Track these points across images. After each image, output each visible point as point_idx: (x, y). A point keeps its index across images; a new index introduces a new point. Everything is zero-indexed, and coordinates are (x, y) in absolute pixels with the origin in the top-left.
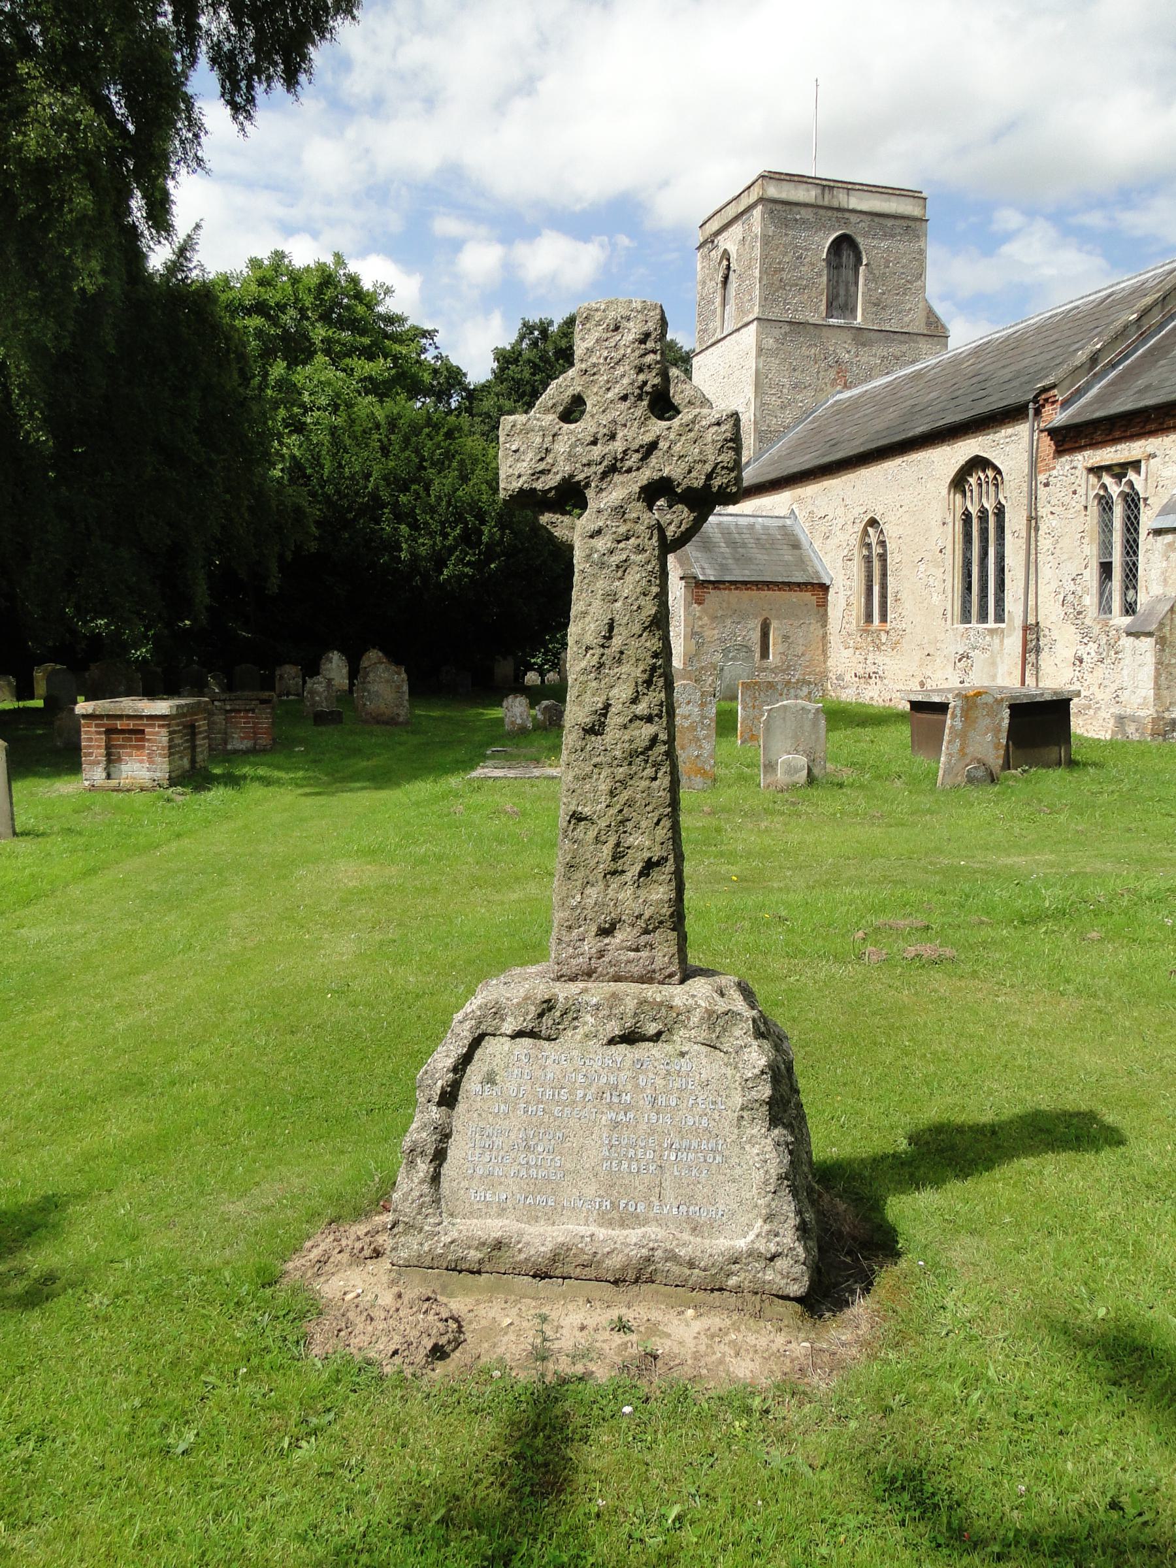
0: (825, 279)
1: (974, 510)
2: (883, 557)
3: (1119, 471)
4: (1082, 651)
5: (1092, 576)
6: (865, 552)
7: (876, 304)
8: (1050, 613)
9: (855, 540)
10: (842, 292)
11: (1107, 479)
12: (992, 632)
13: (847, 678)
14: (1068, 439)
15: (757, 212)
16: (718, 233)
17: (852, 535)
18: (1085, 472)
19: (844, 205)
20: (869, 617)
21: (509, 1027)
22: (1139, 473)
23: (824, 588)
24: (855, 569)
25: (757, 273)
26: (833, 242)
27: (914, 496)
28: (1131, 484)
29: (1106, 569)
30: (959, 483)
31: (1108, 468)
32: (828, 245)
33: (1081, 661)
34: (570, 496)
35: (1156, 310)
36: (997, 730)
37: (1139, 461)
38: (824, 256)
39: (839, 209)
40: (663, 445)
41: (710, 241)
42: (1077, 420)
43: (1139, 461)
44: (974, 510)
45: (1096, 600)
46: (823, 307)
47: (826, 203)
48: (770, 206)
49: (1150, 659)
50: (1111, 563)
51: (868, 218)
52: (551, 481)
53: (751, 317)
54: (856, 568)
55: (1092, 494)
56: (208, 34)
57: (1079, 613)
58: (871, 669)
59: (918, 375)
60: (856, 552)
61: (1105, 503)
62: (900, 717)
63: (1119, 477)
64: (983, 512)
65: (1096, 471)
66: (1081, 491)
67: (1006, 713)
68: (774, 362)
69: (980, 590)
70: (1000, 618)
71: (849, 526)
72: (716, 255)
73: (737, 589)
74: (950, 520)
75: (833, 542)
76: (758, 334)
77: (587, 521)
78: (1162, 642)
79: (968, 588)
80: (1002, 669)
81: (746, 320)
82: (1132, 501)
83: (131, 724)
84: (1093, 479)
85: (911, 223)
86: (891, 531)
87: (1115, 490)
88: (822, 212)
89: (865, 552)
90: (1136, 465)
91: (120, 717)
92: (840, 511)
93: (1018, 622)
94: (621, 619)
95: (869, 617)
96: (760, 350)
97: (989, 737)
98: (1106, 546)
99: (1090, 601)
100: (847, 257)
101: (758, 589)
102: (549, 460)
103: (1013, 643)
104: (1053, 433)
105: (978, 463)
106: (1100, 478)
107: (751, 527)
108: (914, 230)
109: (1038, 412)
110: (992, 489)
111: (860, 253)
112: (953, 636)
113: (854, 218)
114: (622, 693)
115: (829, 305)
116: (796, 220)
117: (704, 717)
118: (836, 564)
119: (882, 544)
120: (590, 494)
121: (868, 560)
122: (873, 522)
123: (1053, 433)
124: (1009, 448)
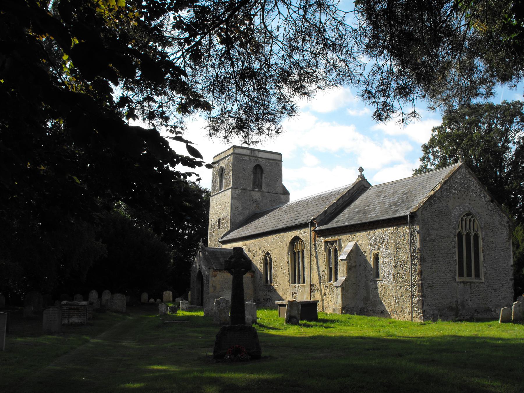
0: (252, 177)
10: (257, 181)
12: (302, 286)
13: (261, 300)
14: (320, 233)
19: (257, 156)
25: (231, 174)
29: (330, 269)
31: (330, 242)
35: (341, 200)
36: (298, 310)
39: (256, 157)
46: (252, 185)
47: (252, 155)
48: (235, 155)
51: (264, 160)
53: (229, 187)
64: (299, 252)
67: (300, 306)
68: (236, 201)
69: (296, 277)
75: (256, 258)
76: (231, 192)
80: (305, 297)
83: (75, 307)
88: (251, 158)
91: (73, 305)
93: (309, 283)
96: (232, 198)
97: (296, 312)
100: (259, 171)
103: (308, 289)
104: (316, 231)
113: (260, 160)
115: (254, 185)
117: (226, 306)
118: (257, 262)
122: (268, 253)
123: (316, 231)
124: (304, 234)
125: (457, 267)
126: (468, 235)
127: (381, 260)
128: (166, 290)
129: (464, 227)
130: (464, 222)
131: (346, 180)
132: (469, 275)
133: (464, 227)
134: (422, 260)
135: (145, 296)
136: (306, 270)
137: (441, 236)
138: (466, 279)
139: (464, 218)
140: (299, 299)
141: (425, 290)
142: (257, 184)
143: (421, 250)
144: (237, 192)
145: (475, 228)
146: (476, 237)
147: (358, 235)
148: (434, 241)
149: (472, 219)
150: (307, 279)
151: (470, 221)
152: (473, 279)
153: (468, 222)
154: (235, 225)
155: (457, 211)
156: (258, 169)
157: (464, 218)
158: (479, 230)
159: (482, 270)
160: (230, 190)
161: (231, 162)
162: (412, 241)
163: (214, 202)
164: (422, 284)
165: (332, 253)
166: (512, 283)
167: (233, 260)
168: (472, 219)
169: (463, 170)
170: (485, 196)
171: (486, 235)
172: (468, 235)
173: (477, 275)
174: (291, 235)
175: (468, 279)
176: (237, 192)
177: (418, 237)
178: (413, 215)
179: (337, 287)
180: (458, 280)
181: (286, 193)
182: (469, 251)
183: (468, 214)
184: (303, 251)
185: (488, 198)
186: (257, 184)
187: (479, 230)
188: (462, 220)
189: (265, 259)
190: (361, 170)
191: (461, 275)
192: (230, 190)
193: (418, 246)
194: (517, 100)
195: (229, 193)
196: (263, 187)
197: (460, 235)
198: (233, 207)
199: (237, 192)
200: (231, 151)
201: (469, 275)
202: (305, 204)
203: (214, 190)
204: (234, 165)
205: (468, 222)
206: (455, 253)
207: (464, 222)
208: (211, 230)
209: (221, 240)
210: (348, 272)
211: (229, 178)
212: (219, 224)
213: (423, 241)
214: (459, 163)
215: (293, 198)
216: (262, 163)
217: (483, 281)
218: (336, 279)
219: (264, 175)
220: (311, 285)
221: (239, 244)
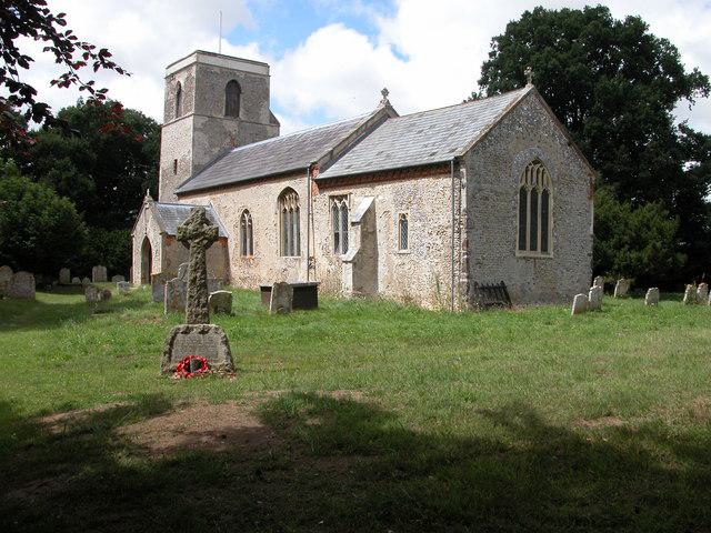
1: (529, 189)
2: (251, 227)
3: (340, 198)
5: (331, 239)
8: (319, 253)
14: (323, 185)
15: (194, 68)
16: (176, 73)
23: (226, 239)
27: (263, 202)
29: (337, 235)
30: (282, 197)
41: (170, 77)
44: (529, 189)
49: (351, 271)
59: (265, 146)
61: (335, 208)
62: (255, 293)
64: (291, 209)
65: (332, 197)
68: (200, 134)
69: (290, 244)
70: (299, 254)
72: (174, 83)
75: (229, 219)
78: (355, 264)
79: (245, 240)
80: (301, 275)
82: (344, 208)
86: (254, 215)
87: (339, 205)
95: (245, 253)
98: (337, 227)
99: (332, 248)
103: (304, 264)
104: (316, 181)
105: (289, 190)
109: (311, 172)
112: (279, 263)
118: (229, 229)
119: (250, 221)
121: (244, 227)
122: (246, 211)
123: (316, 181)
124: (301, 185)
125: (518, 235)
126: (534, 192)
127: (410, 225)
128: (96, 265)
129: (540, 181)
130: (529, 173)
131: (361, 108)
132: (533, 248)
133: (540, 181)
134: (469, 228)
135: (65, 273)
136: (306, 244)
137: (496, 193)
138: (527, 253)
139: (530, 167)
140: (290, 281)
141: (471, 269)
142: (232, 111)
143: (468, 211)
144: (203, 120)
145: (545, 182)
146: (546, 195)
147: (379, 188)
148: (487, 199)
149: (541, 169)
150: (304, 249)
151: (538, 172)
152: (538, 253)
153: (535, 173)
154: (198, 170)
155: (522, 157)
156: (234, 87)
157: (530, 167)
158: (550, 185)
159: (551, 241)
160: (191, 118)
161: (194, 74)
162: (455, 200)
163: (167, 137)
164: (467, 260)
165: (340, 212)
166: (590, 259)
167: (190, 227)
168: (541, 169)
169: (533, 98)
170: (560, 137)
171: (560, 192)
172: (534, 192)
173: (544, 249)
174: (278, 187)
175: (532, 254)
176: (202, 121)
177: (464, 192)
178: (458, 161)
179: (346, 262)
180: (517, 254)
181: (275, 123)
182: (533, 212)
183: (535, 162)
184: (298, 209)
185: (565, 140)
186: (232, 111)
187: (550, 185)
188: (527, 171)
189: (243, 220)
190: (385, 92)
191: (522, 247)
192: (191, 118)
193: (464, 206)
194: (480, 70)
195: (189, 122)
196: (241, 113)
197: (523, 192)
198: (197, 143)
199: (203, 120)
200: (192, 60)
201: (533, 248)
202: (299, 143)
203: (167, 117)
204: (198, 80)
205: (535, 173)
206: (515, 216)
207: (529, 173)
208: (555, 198)
209: (178, 191)
210: (362, 241)
211: (190, 98)
212: (176, 167)
213: (471, 198)
214: (529, 87)
215: (288, 129)
216: (240, 79)
217: (552, 256)
218: (345, 251)
219: (242, 96)
220: (310, 259)
221: (203, 201)
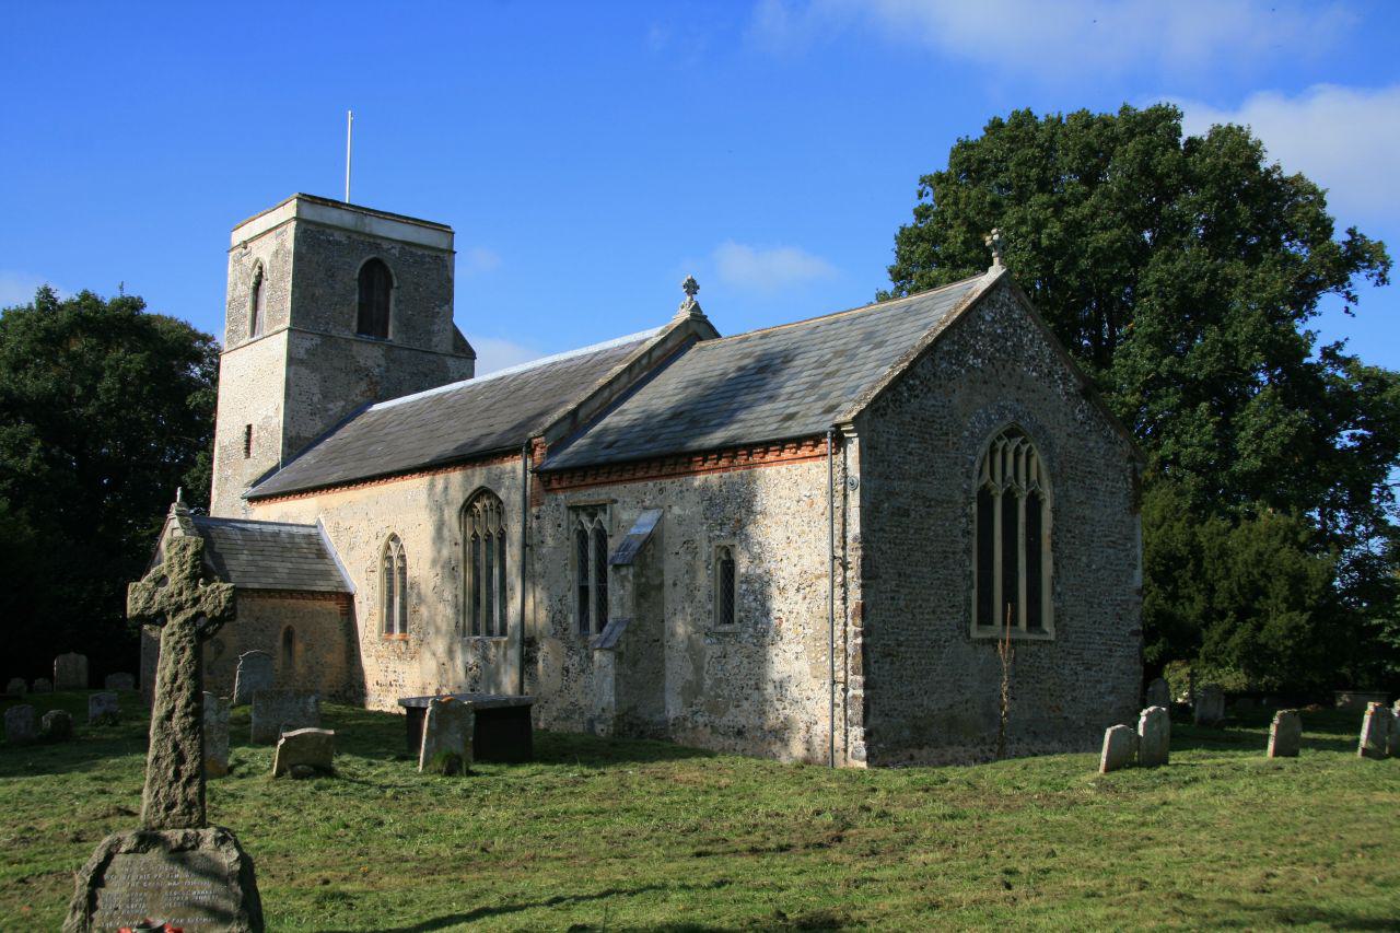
0: (357, 297)
3: (593, 510)
4: (568, 663)
6: (387, 565)
7: (406, 325)
9: (378, 555)
11: (584, 519)
17: (374, 550)
18: (566, 511)
20: (390, 628)
21: (123, 849)
22: (605, 513)
24: (378, 580)
26: (361, 270)
28: (600, 522)
31: (584, 508)
32: (360, 266)
33: (568, 671)
34: (160, 618)
37: (605, 505)
38: (356, 276)
40: (203, 599)
42: (567, 464)
43: (605, 505)
45: (577, 617)
46: (354, 324)
50: (587, 587)
52: (153, 610)
54: (377, 578)
55: (572, 528)
56: (253, 755)
57: (565, 630)
58: (392, 677)
60: (378, 563)
61: (582, 535)
63: (592, 516)
64: (489, 535)
65: (574, 509)
66: (564, 524)
68: (304, 371)
71: (373, 540)
73: (259, 597)
74: (460, 541)
77: (166, 630)
81: (277, 328)
82: (602, 537)
84: (573, 517)
85: (439, 254)
87: (589, 527)
89: (387, 565)
90: (603, 507)
92: (364, 524)
94: (181, 671)
101: (281, 597)
102: (152, 603)
106: (578, 515)
107: (277, 534)
108: (443, 260)
110: (495, 517)
111: (391, 276)
114: (181, 703)
116: (329, 241)
119: (403, 558)
120: (169, 617)
121: (389, 572)
122: (394, 538)
